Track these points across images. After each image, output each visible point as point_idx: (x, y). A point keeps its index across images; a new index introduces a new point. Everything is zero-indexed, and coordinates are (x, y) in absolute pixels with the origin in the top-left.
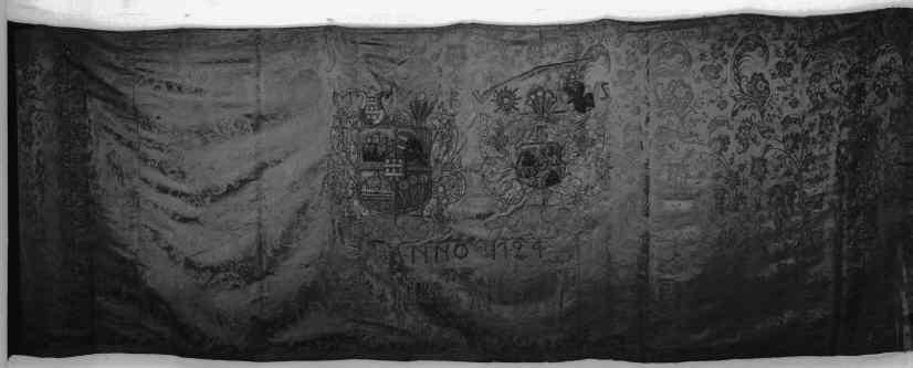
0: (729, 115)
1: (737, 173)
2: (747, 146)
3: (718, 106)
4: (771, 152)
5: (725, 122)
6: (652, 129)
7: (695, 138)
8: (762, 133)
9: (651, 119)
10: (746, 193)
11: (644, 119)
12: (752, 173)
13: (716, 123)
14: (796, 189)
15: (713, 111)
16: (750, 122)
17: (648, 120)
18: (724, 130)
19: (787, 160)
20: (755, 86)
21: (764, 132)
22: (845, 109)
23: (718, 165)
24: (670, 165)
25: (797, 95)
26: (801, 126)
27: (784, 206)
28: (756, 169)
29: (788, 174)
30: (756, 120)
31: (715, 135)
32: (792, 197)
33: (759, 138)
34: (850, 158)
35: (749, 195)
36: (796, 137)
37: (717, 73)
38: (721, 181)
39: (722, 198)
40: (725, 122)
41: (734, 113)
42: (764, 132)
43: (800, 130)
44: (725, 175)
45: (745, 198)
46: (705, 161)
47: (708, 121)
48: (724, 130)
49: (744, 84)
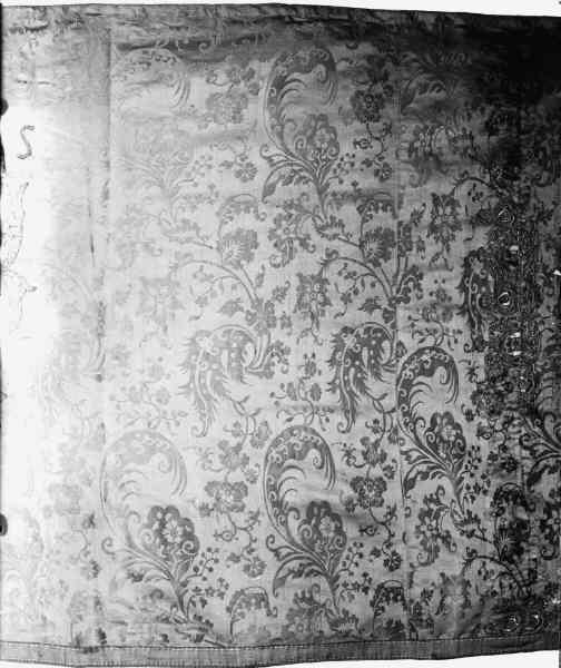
0: (269, 588)
1: (269, 304)
2: (291, 254)
3: (247, 568)
4: (335, 267)
5: (248, 206)
6: (115, 210)
7: (192, 233)
8: (320, 230)
9: (111, 194)
10: (289, 342)
11: (98, 194)
12: (300, 304)
13: (235, 204)
14: (385, 337)
15: (236, 578)
16: (299, 207)
17: (106, 195)
18: (247, 222)
19: (369, 280)
20: (316, 527)
21: (323, 228)
22: (481, 188)
23: (234, 287)
24: (144, 281)
25: (390, 159)
26: (395, 216)
27: (359, 369)
28: (307, 298)
29: (370, 305)
30: (302, 63)
31: (230, 228)
32: (377, 350)
33: (315, 238)
34: (490, 278)
35: (293, 346)
36: (385, 238)
37: (238, 498)
38: (239, 318)
39: (240, 350)
40: (262, 599)
41: (280, 582)
42: (323, 228)
43: (392, 224)
44: (247, 306)
45: (288, 351)
46: (209, 278)
47: (229, 594)
48: (247, 222)
49: (293, 524)
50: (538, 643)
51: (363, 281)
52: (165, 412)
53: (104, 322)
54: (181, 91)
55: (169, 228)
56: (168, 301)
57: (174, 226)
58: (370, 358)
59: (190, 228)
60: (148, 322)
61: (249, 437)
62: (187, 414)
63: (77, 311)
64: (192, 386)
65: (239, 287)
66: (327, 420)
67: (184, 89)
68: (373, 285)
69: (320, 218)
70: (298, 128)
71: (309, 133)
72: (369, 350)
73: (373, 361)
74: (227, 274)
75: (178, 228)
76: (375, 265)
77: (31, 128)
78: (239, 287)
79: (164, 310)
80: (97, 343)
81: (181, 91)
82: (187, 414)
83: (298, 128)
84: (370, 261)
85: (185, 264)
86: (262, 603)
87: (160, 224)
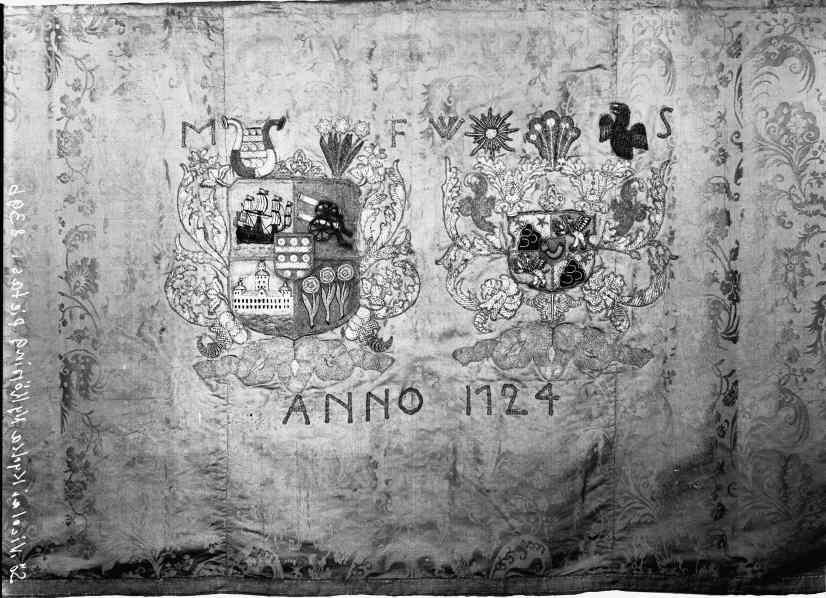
9: (745, 172)
50: (671, 582)
51: (71, 312)
52: (795, 370)
53: (739, 290)
54: (806, 78)
55: (798, 202)
56: (798, 269)
57: (803, 200)
58: (79, 379)
59: (818, 202)
60: (779, 289)
61: (722, 397)
62: (813, 371)
63: (716, 280)
64: (819, 345)
65: (87, 317)
66: (805, 380)
67: (810, 76)
68: (82, 317)
69: (796, 196)
70: (770, 117)
71: (781, 120)
72: (79, 374)
73: (82, 383)
74: (76, 304)
75: (806, 203)
76: (83, 298)
77: (670, 110)
78: (87, 317)
79: (794, 278)
80: (733, 307)
81: (806, 78)
82: (813, 371)
83: (770, 117)
84: (78, 294)
85: (813, 235)
86: (722, 544)
87: (790, 198)
